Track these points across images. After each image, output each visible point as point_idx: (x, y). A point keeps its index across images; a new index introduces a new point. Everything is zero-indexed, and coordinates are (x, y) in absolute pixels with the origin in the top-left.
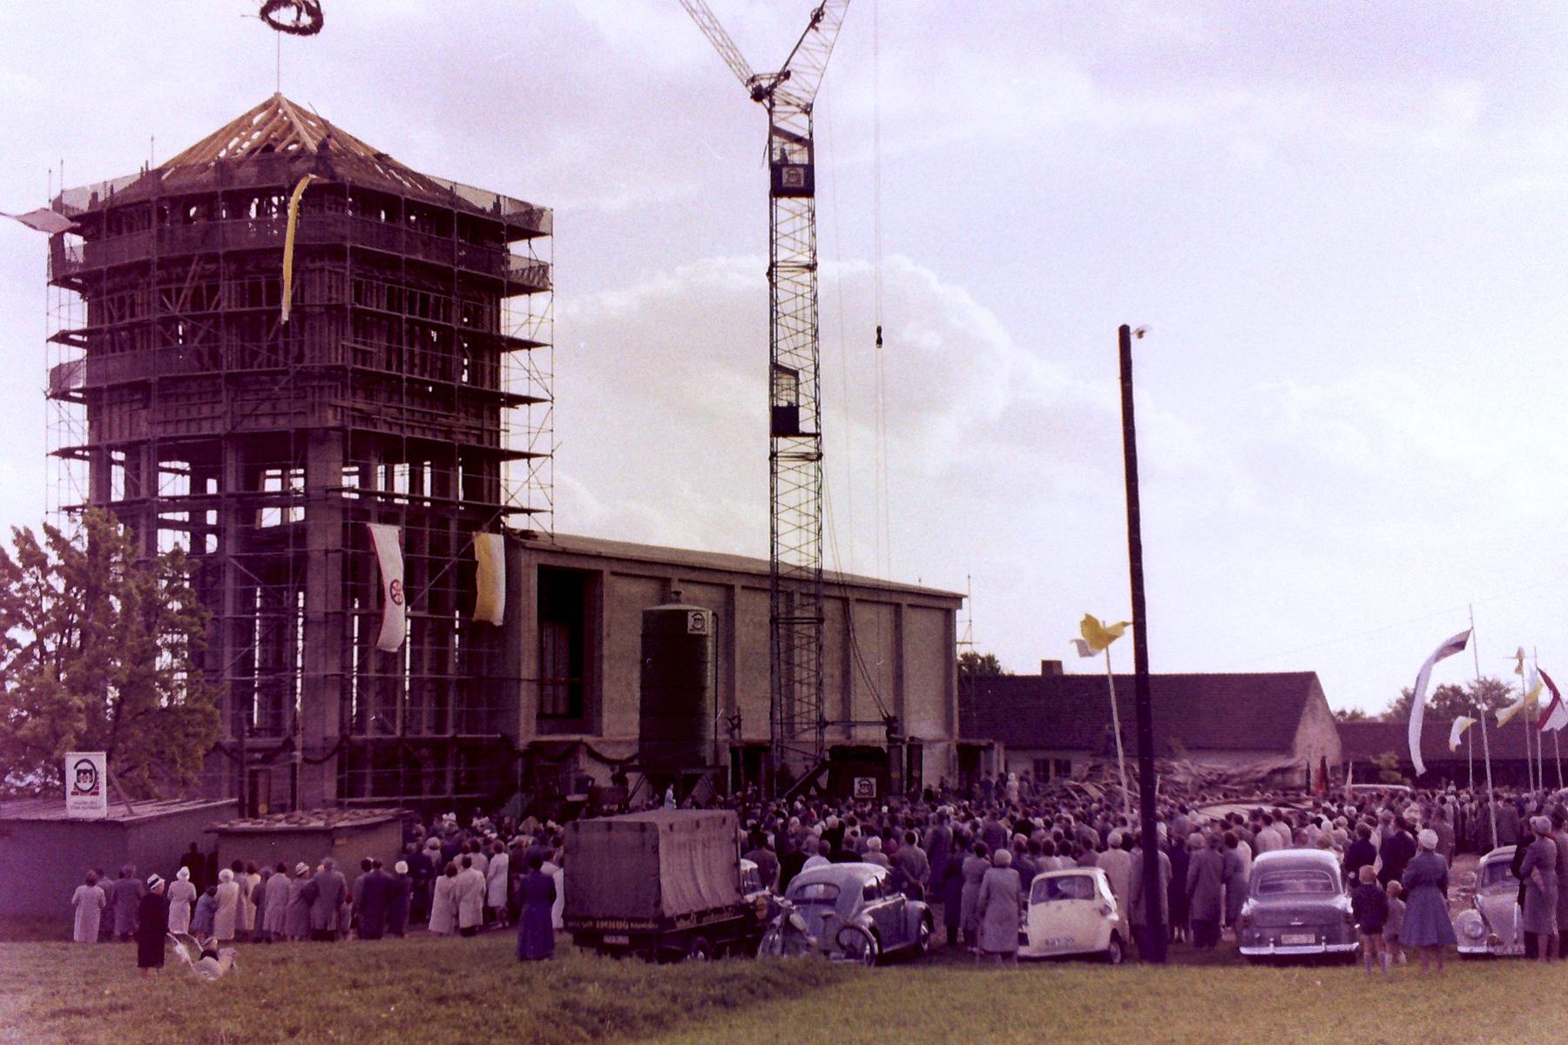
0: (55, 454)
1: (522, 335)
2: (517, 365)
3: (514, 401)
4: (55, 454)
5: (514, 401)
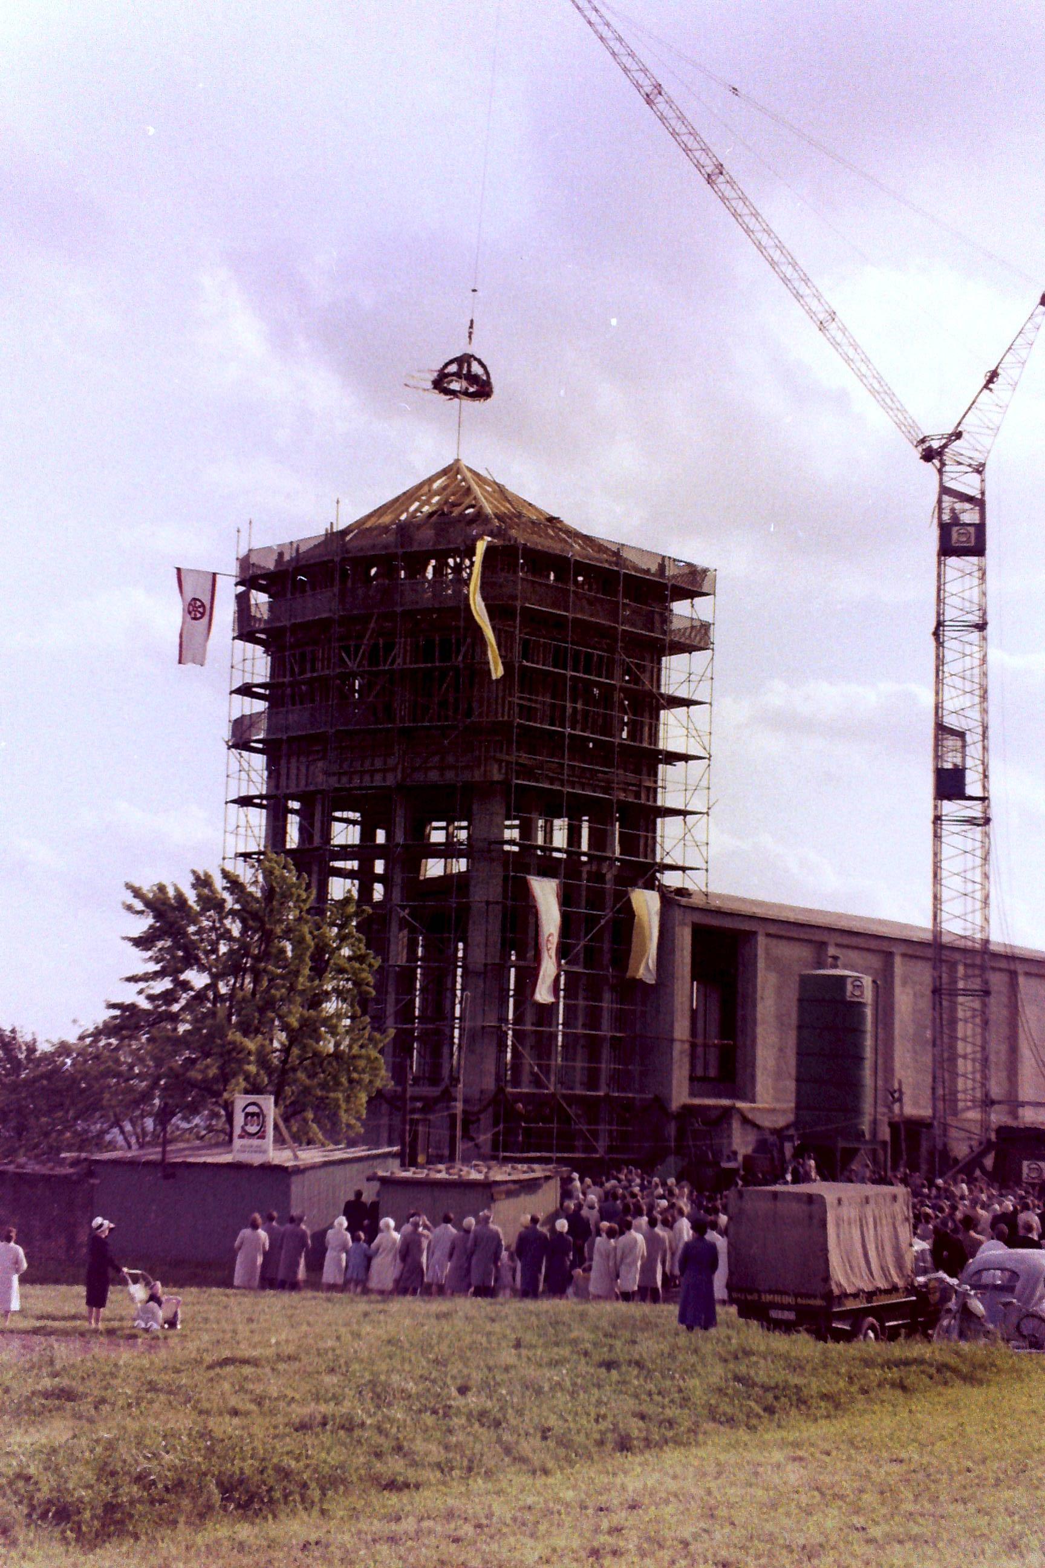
0: (234, 802)
1: (682, 693)
2: (675, 723)
3: (673, 758)
4: (234, 802)
5: (673, 758)
